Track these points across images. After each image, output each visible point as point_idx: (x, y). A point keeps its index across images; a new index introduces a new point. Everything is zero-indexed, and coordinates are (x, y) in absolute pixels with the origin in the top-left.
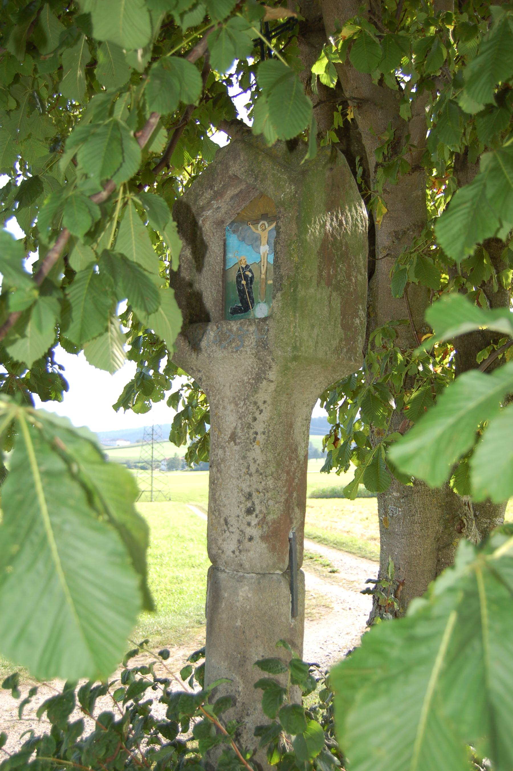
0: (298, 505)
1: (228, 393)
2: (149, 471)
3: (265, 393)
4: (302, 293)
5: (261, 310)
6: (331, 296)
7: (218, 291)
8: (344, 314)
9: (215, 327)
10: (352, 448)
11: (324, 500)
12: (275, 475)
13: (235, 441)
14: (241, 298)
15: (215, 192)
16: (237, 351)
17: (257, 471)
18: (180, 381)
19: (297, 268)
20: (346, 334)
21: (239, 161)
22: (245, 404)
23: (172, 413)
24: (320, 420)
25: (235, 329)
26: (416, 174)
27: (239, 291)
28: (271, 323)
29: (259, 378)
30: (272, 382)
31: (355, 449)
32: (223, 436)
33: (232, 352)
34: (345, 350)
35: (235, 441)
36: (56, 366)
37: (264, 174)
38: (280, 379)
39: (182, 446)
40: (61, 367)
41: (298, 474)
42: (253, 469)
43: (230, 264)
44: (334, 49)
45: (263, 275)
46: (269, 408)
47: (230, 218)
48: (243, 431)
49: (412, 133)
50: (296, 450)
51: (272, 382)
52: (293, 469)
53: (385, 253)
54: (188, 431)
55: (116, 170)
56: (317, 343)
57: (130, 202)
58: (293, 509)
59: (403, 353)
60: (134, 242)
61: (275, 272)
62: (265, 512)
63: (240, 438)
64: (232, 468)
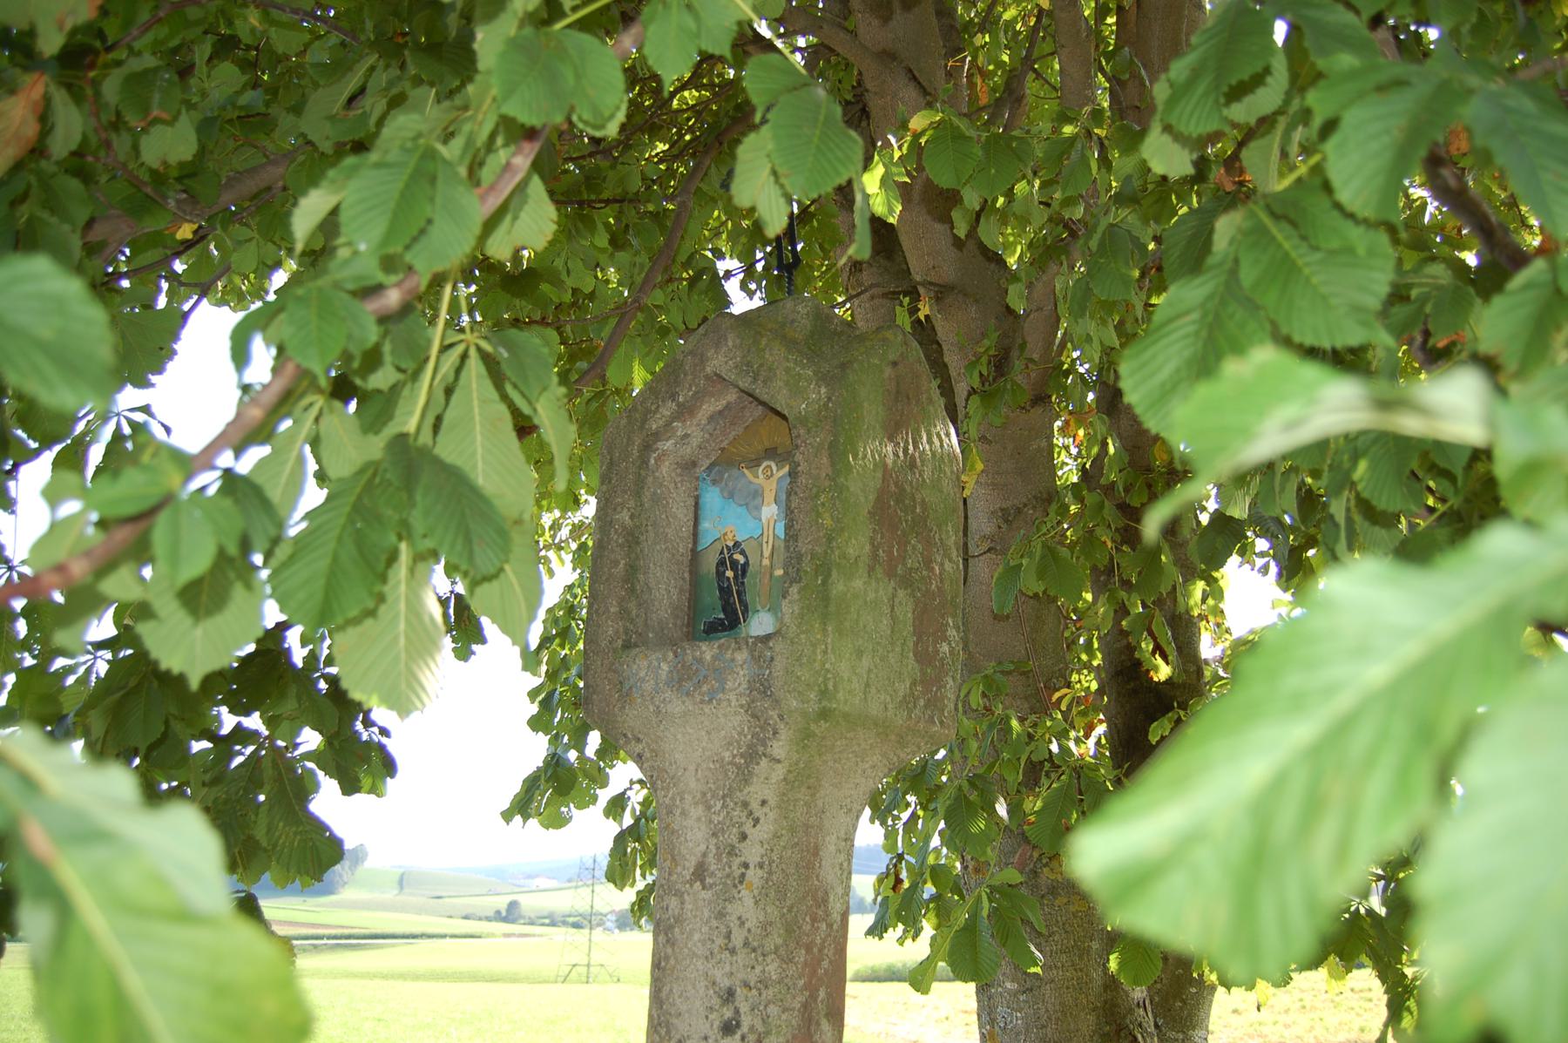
0: (827, 1015)
1: (692, 783)
2: (586, 931)
3: (766, 784)
4: (838, 587)
5: (760, 623)
6: (894, 596)
7: (681, 591)
8: (919, 633)
9: (671, 655)
10: (926, 896)
11: (876, 984)
12: (782, 952)
13: (702, 881)
14: (719, 600)
15: (679, 405)
16: (710, 701)
17: (746, 944)
18: (623, 774)
19: (830, 540)
20: (923, 673)
21: (724, 349)
22: (724, 806)
23: (612, 828)
24: (868, 850)
25: (708, 657)
26: (1038, 410)
27: (721, 589)
28: (778, 646)
29: (752, 755)
30: (779, 761)
31: (933, 898)
32: (679, 869)
33: (702, 702)
34: (922, 702)
35: (702, 881)
36: (375, 730)
37: (770, 369)
38: (795, 756)
39: (627, 888)
40: (384, 732)
41: (830, 951)
42: (738, 939)
43: (705, 542)
44: (897, 154)
45: (765, 560)
46: (772, 815)
47: (707, 457)
48: (719, 860)
49: (1028, 339)
50: (825, 901)
51: (779, 761)
52: (818, 941)
53: (985, 546)
54: (639, 862)
55: (415, 232)
56: (867, 685)
57: (473, 352)
58: (818, 1024)
59: (1022, 720)
60: (479, 438)
61: (787, 548)
62: (761, 1029)
63: (712, 874)
64: (696, 937)
